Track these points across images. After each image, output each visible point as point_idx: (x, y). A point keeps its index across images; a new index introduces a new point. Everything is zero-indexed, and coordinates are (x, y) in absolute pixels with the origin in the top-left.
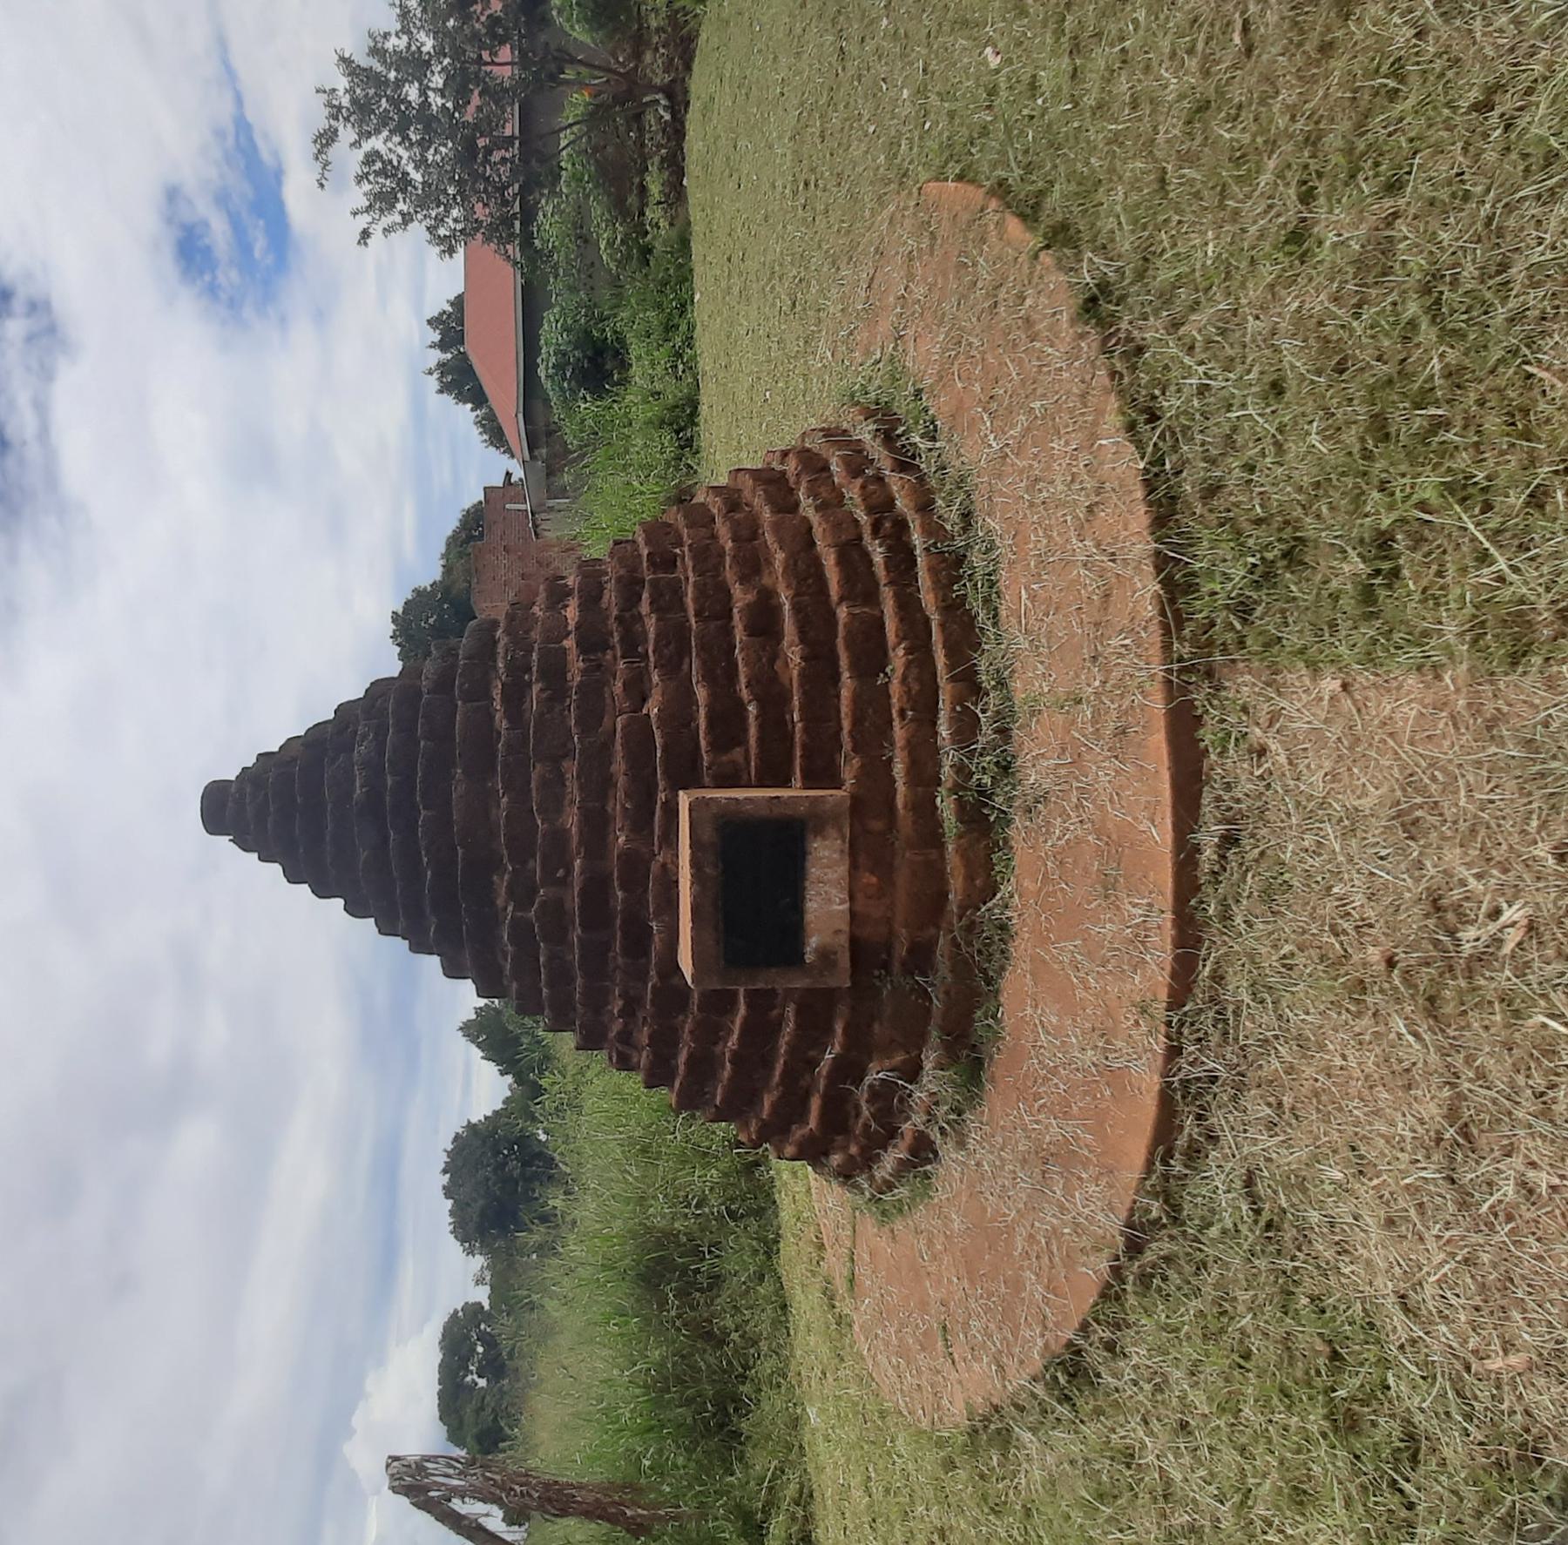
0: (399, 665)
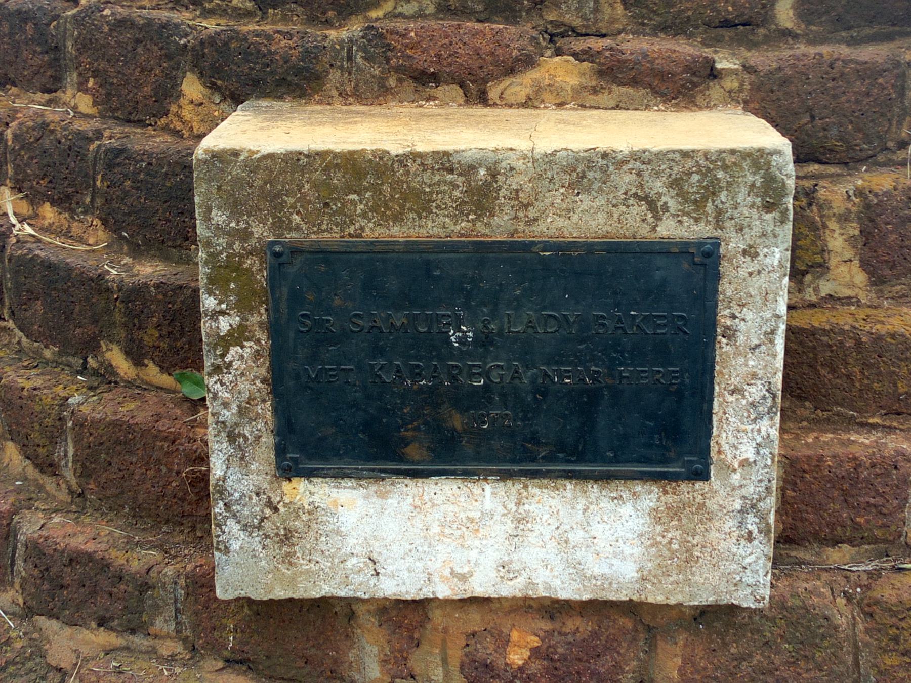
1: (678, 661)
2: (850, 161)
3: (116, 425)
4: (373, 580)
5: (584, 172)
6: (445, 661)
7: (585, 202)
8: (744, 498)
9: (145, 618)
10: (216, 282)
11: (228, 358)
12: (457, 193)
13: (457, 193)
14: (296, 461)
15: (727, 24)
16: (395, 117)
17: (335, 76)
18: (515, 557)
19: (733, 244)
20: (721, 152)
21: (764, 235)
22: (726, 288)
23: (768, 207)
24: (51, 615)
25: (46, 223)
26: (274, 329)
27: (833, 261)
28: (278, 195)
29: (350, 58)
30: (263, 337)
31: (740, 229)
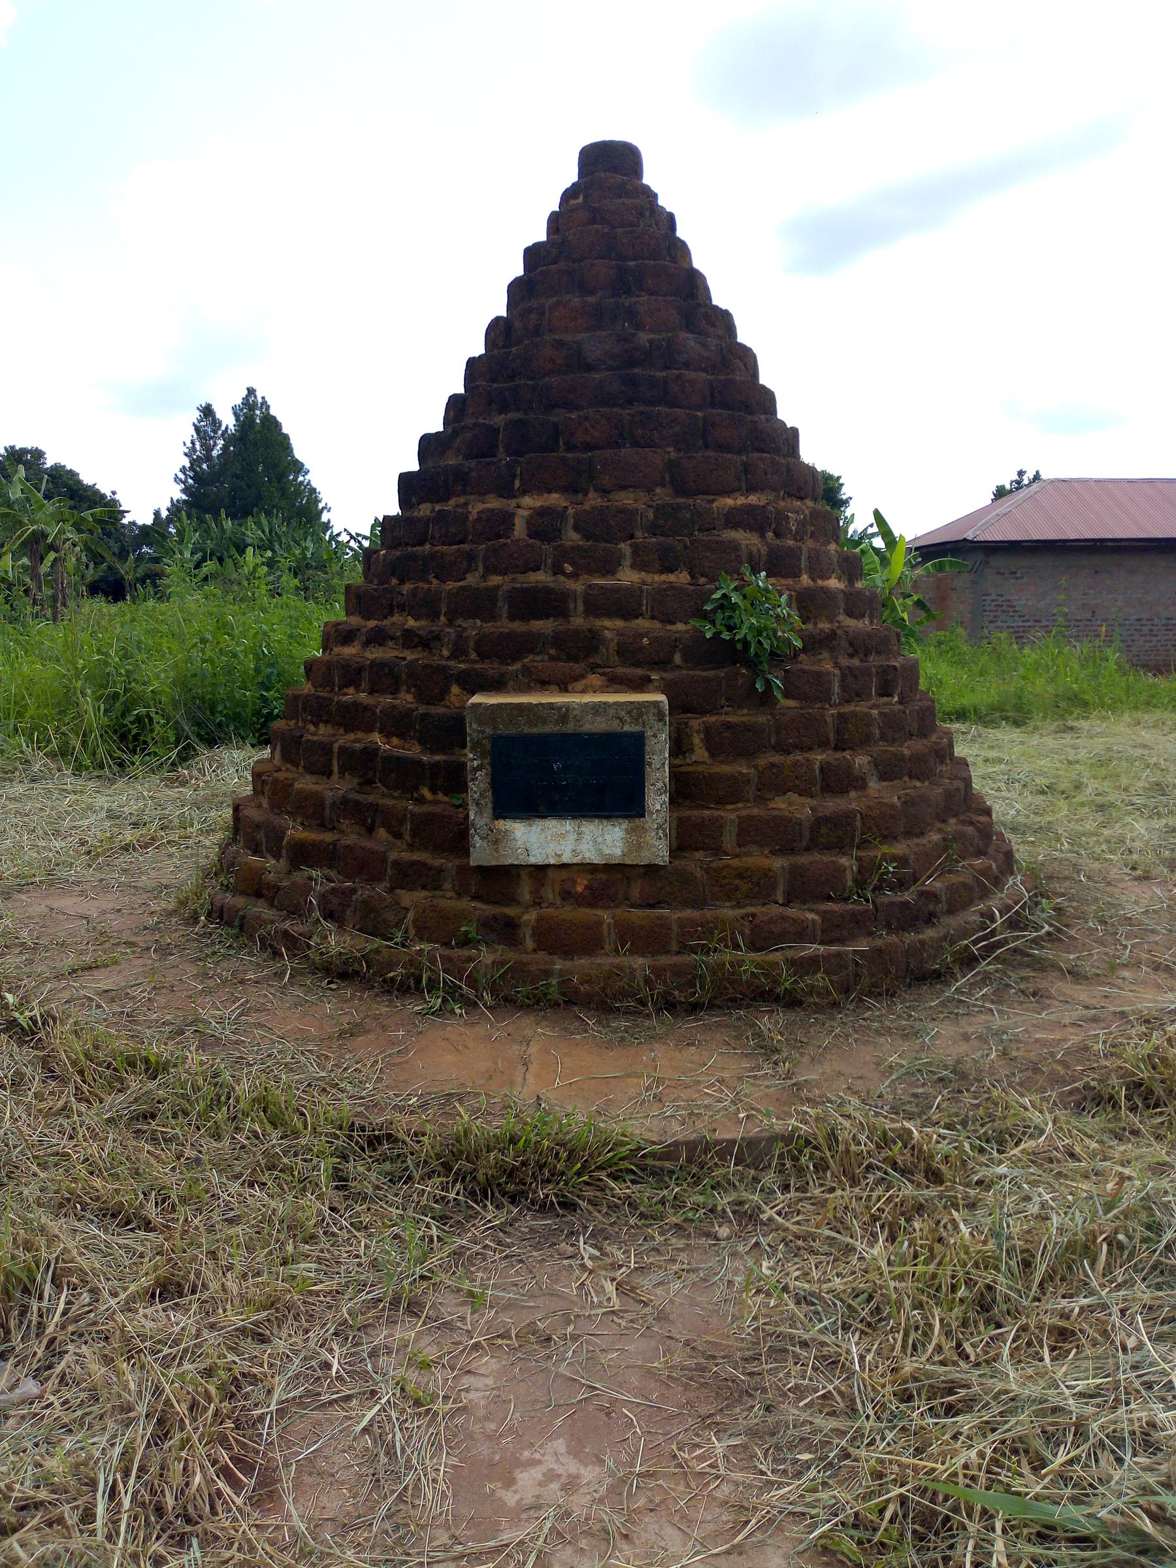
2: (703, 713)
3: (428, 813)
7: (598, 719)
10: (473, 749)
17: (511, 683)
19: (649, 733)
22: (647, 749)
23: (660, 720)
24: (403, 888)
26: (493, 765)
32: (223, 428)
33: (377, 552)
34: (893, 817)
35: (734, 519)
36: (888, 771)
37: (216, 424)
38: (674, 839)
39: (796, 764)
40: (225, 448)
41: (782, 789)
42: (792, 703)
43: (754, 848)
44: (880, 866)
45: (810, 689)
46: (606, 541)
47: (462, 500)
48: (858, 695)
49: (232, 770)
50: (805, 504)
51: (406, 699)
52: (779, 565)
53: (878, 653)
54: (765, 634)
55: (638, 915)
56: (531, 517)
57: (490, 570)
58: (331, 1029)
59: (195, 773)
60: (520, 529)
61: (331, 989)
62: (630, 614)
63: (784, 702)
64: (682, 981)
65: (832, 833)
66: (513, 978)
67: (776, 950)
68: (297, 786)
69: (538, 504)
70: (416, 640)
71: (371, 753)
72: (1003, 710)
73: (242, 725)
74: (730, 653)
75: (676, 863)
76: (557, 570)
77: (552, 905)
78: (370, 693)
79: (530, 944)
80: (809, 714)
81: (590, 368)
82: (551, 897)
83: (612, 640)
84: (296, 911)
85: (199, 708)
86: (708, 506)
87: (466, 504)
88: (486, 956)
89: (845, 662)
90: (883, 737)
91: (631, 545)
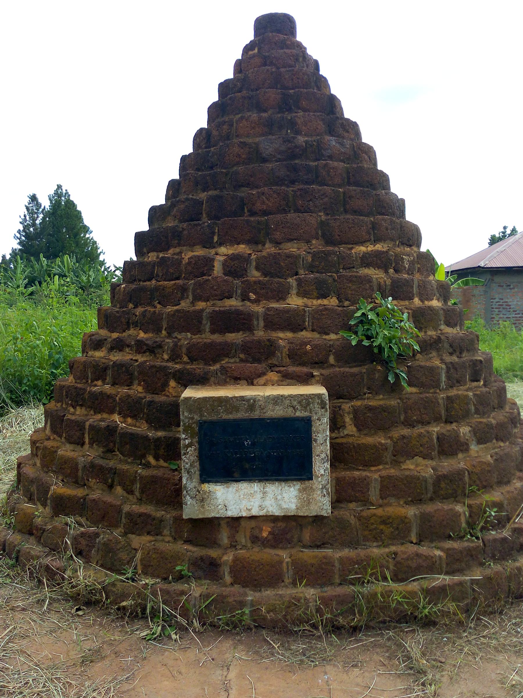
0: (191, 151)
1: (309, 534)
2: (351, 398)
3: (153, 476)
4: (226, 512)
5: (277, 400)
6: (245, 537)
7: (277, 408)
8: (322, 485)
9: (161, 530)
10: (185, 431)
11: (188, 451)
12: (246, 406)
13: (246, 406)
14: (205, 478)
15: (316, 363)
16: (229, 389)
17: (212, 379)
18: (263, 504)
19: (315, 417)
20: (310, 394)
21: (322, 415)
22: (314, 429)
23: (322, 408)
25: (129, 423)
26: (200, 443)
27: (347, 425)
28: (201, 408)
29: (217, 374)
30: (197, 445)
31: (316, 413)
32: (42, 207)
33: (119, 285)
34: (489, 471)
35: (367, 261)
36: (483, 436)
37: (39, 205)
38: (333, 494)
39: (420, 435)
40: (44, 219)
41: (411, 455)
42: (414, 390)
43: (392, 500)
44: (485, 512)
45: (425, 379)
46: (279, 277)
47: (177, 250)
48: (458, 382)
49: (30, 423)
50: (412, 249)
51: (137, 390)
52: (399, 291)
53: (468, 351)
54: (394, 341)
55: (309, 555)
56: (225, 261)
57: (197, 298)
58: (75, 655)
59: (6, 425)
60: (218, 269)
61: (78, 615)
62: (297, 328)
63: (409, 389)
64: (345, 608)
65: (449, 487)
66: (215, 608)
67: (414, 580)
68: (60, 452)
69: (230, 252)
70: (145, 348)
71: (111, 430)
72: (514, 371)
73: (39, 392)
74: (371, 355)
75: (336, 513)
76: (245, 298)
77: (244, 547)
78: (112, 385)
79: (228, 579)
80: (427, 397)
81: (265, 160)
82: (243, 541)
83: (285, 347)
84: (54, 549)
85: (12, 381)
86: (349, 252)
87: (181, 253)
88: (196, 589)
89: (448, 359)
90: (477, 412)
91: (296, 280)
